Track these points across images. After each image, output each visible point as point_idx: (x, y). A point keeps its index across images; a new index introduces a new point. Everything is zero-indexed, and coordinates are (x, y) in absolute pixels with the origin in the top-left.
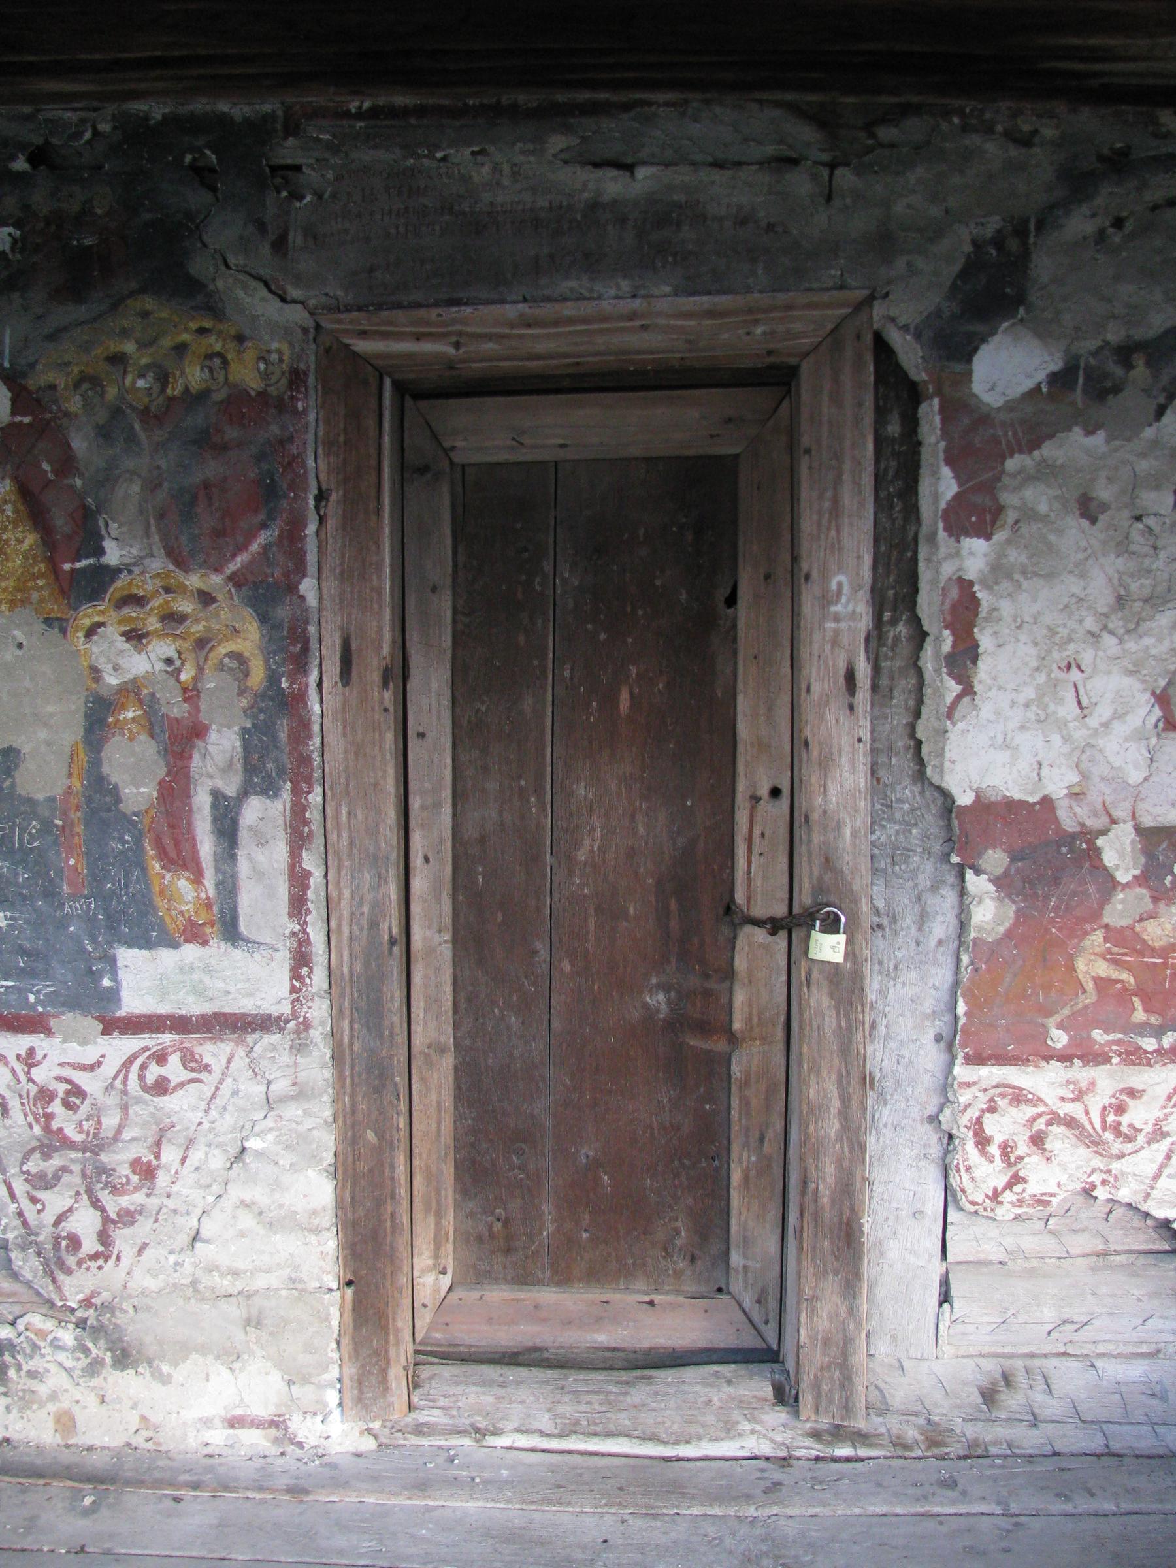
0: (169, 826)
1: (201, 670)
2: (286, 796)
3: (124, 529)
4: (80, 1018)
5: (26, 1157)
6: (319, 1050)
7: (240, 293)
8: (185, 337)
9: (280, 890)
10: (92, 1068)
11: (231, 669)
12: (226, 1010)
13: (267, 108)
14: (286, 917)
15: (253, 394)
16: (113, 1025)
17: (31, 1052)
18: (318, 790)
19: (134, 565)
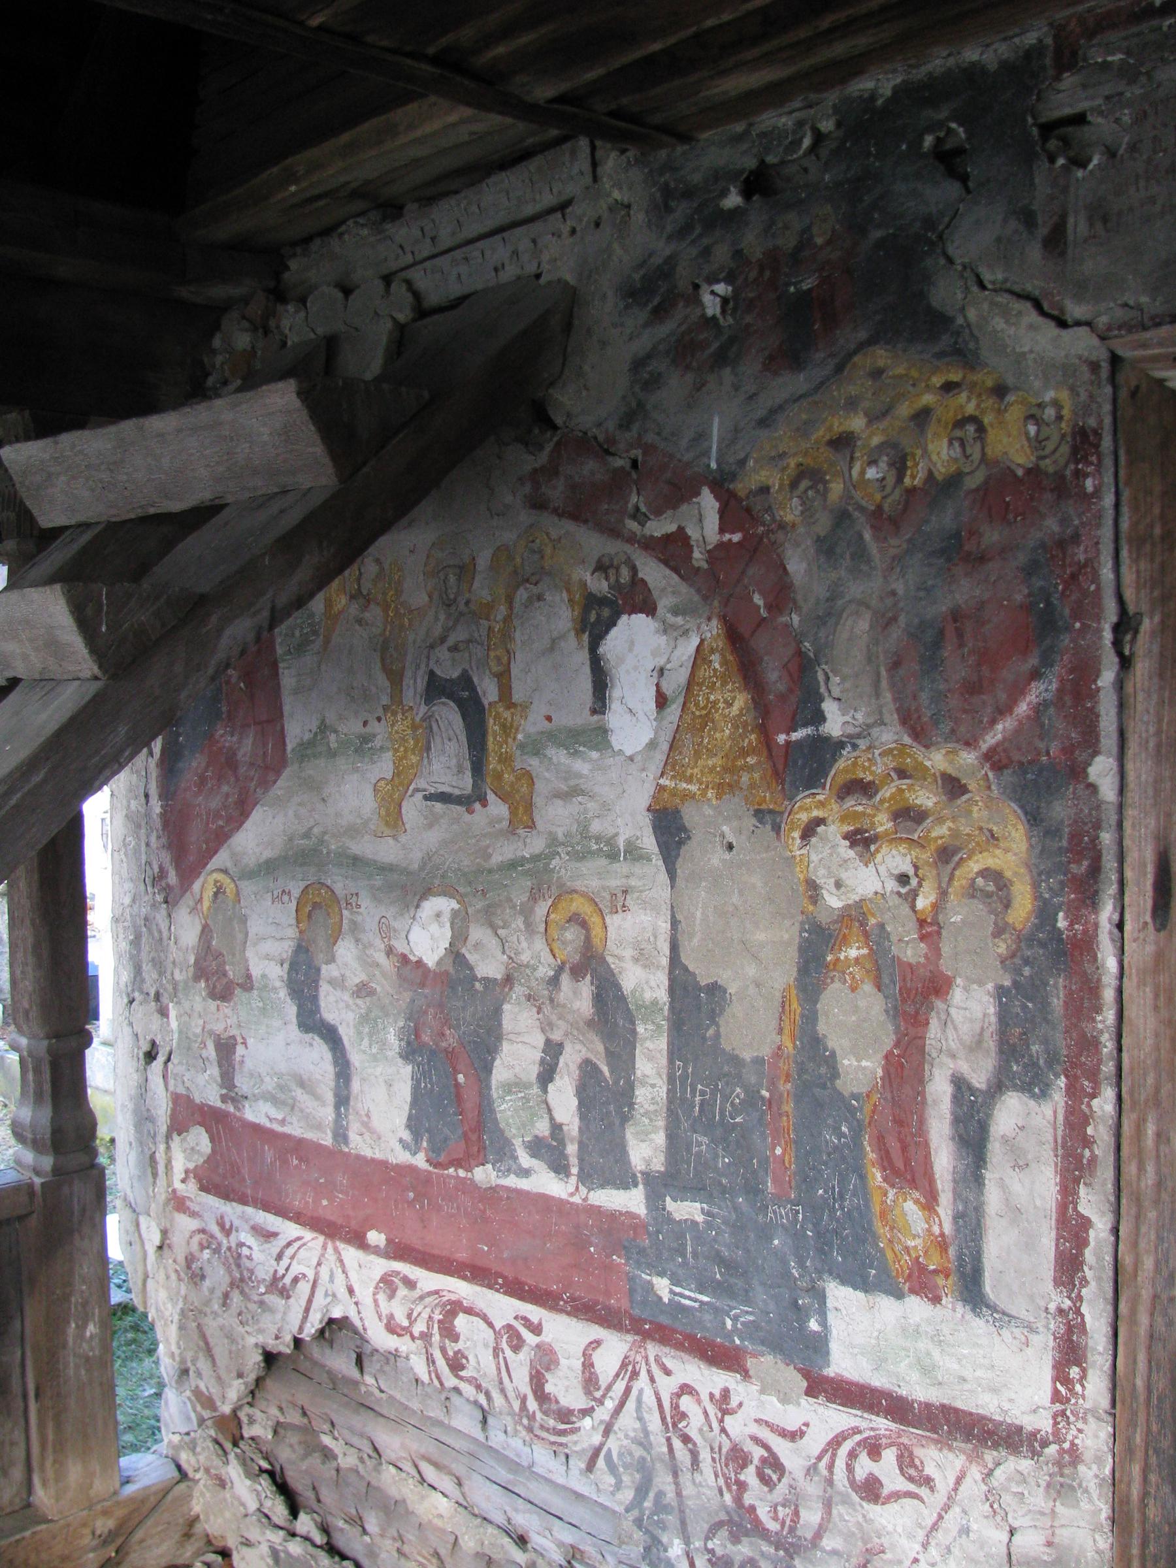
0: (895, 1121)
1: (943, 894)
2: (1059, 1097)
3: (847, 685)
4: (781, 1365)
5: (710, 1535)
6: (1090, 1500)
7: (998, 323)
8: (928, 399)
9: (1044, 1240)
10: (793, 1436)
11: (989, 895)
12: (959, 1404)
13: (1031, 38)
14: (1051, 1285)
15: (1020, 473)
16: (823, 1387)
17: (726, 1394)
18: (1109, 1093)
19: (859, 736)
